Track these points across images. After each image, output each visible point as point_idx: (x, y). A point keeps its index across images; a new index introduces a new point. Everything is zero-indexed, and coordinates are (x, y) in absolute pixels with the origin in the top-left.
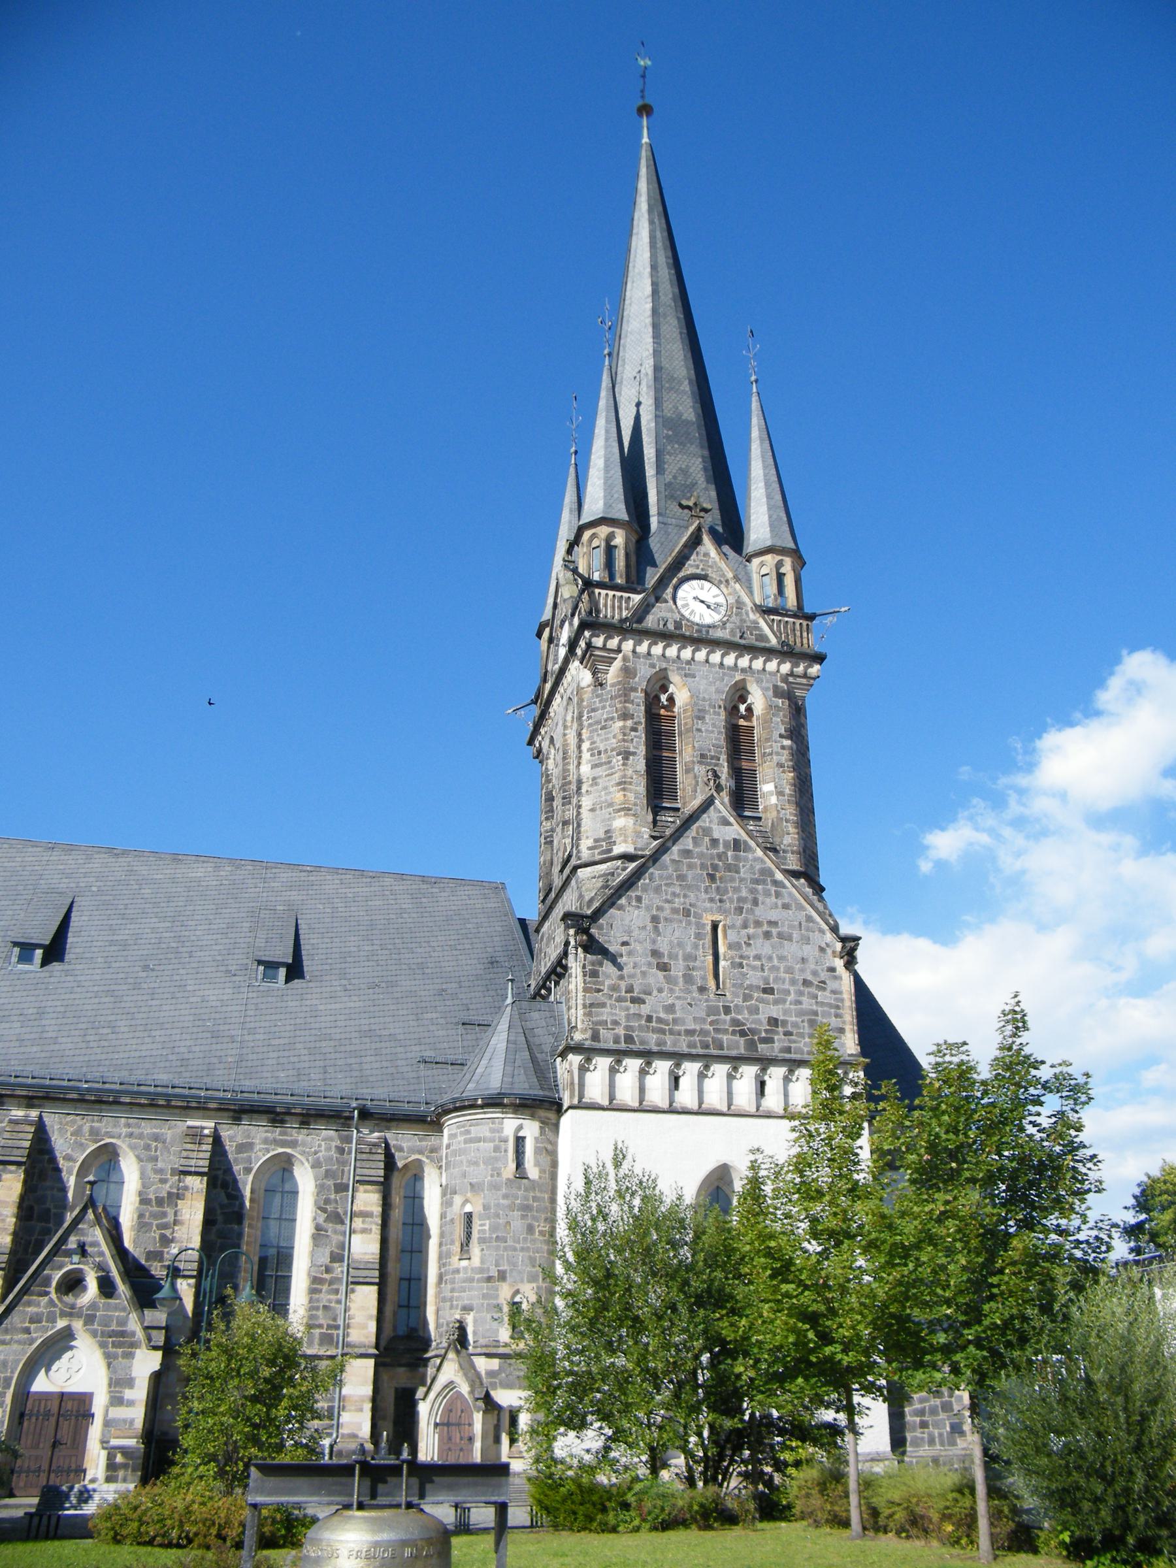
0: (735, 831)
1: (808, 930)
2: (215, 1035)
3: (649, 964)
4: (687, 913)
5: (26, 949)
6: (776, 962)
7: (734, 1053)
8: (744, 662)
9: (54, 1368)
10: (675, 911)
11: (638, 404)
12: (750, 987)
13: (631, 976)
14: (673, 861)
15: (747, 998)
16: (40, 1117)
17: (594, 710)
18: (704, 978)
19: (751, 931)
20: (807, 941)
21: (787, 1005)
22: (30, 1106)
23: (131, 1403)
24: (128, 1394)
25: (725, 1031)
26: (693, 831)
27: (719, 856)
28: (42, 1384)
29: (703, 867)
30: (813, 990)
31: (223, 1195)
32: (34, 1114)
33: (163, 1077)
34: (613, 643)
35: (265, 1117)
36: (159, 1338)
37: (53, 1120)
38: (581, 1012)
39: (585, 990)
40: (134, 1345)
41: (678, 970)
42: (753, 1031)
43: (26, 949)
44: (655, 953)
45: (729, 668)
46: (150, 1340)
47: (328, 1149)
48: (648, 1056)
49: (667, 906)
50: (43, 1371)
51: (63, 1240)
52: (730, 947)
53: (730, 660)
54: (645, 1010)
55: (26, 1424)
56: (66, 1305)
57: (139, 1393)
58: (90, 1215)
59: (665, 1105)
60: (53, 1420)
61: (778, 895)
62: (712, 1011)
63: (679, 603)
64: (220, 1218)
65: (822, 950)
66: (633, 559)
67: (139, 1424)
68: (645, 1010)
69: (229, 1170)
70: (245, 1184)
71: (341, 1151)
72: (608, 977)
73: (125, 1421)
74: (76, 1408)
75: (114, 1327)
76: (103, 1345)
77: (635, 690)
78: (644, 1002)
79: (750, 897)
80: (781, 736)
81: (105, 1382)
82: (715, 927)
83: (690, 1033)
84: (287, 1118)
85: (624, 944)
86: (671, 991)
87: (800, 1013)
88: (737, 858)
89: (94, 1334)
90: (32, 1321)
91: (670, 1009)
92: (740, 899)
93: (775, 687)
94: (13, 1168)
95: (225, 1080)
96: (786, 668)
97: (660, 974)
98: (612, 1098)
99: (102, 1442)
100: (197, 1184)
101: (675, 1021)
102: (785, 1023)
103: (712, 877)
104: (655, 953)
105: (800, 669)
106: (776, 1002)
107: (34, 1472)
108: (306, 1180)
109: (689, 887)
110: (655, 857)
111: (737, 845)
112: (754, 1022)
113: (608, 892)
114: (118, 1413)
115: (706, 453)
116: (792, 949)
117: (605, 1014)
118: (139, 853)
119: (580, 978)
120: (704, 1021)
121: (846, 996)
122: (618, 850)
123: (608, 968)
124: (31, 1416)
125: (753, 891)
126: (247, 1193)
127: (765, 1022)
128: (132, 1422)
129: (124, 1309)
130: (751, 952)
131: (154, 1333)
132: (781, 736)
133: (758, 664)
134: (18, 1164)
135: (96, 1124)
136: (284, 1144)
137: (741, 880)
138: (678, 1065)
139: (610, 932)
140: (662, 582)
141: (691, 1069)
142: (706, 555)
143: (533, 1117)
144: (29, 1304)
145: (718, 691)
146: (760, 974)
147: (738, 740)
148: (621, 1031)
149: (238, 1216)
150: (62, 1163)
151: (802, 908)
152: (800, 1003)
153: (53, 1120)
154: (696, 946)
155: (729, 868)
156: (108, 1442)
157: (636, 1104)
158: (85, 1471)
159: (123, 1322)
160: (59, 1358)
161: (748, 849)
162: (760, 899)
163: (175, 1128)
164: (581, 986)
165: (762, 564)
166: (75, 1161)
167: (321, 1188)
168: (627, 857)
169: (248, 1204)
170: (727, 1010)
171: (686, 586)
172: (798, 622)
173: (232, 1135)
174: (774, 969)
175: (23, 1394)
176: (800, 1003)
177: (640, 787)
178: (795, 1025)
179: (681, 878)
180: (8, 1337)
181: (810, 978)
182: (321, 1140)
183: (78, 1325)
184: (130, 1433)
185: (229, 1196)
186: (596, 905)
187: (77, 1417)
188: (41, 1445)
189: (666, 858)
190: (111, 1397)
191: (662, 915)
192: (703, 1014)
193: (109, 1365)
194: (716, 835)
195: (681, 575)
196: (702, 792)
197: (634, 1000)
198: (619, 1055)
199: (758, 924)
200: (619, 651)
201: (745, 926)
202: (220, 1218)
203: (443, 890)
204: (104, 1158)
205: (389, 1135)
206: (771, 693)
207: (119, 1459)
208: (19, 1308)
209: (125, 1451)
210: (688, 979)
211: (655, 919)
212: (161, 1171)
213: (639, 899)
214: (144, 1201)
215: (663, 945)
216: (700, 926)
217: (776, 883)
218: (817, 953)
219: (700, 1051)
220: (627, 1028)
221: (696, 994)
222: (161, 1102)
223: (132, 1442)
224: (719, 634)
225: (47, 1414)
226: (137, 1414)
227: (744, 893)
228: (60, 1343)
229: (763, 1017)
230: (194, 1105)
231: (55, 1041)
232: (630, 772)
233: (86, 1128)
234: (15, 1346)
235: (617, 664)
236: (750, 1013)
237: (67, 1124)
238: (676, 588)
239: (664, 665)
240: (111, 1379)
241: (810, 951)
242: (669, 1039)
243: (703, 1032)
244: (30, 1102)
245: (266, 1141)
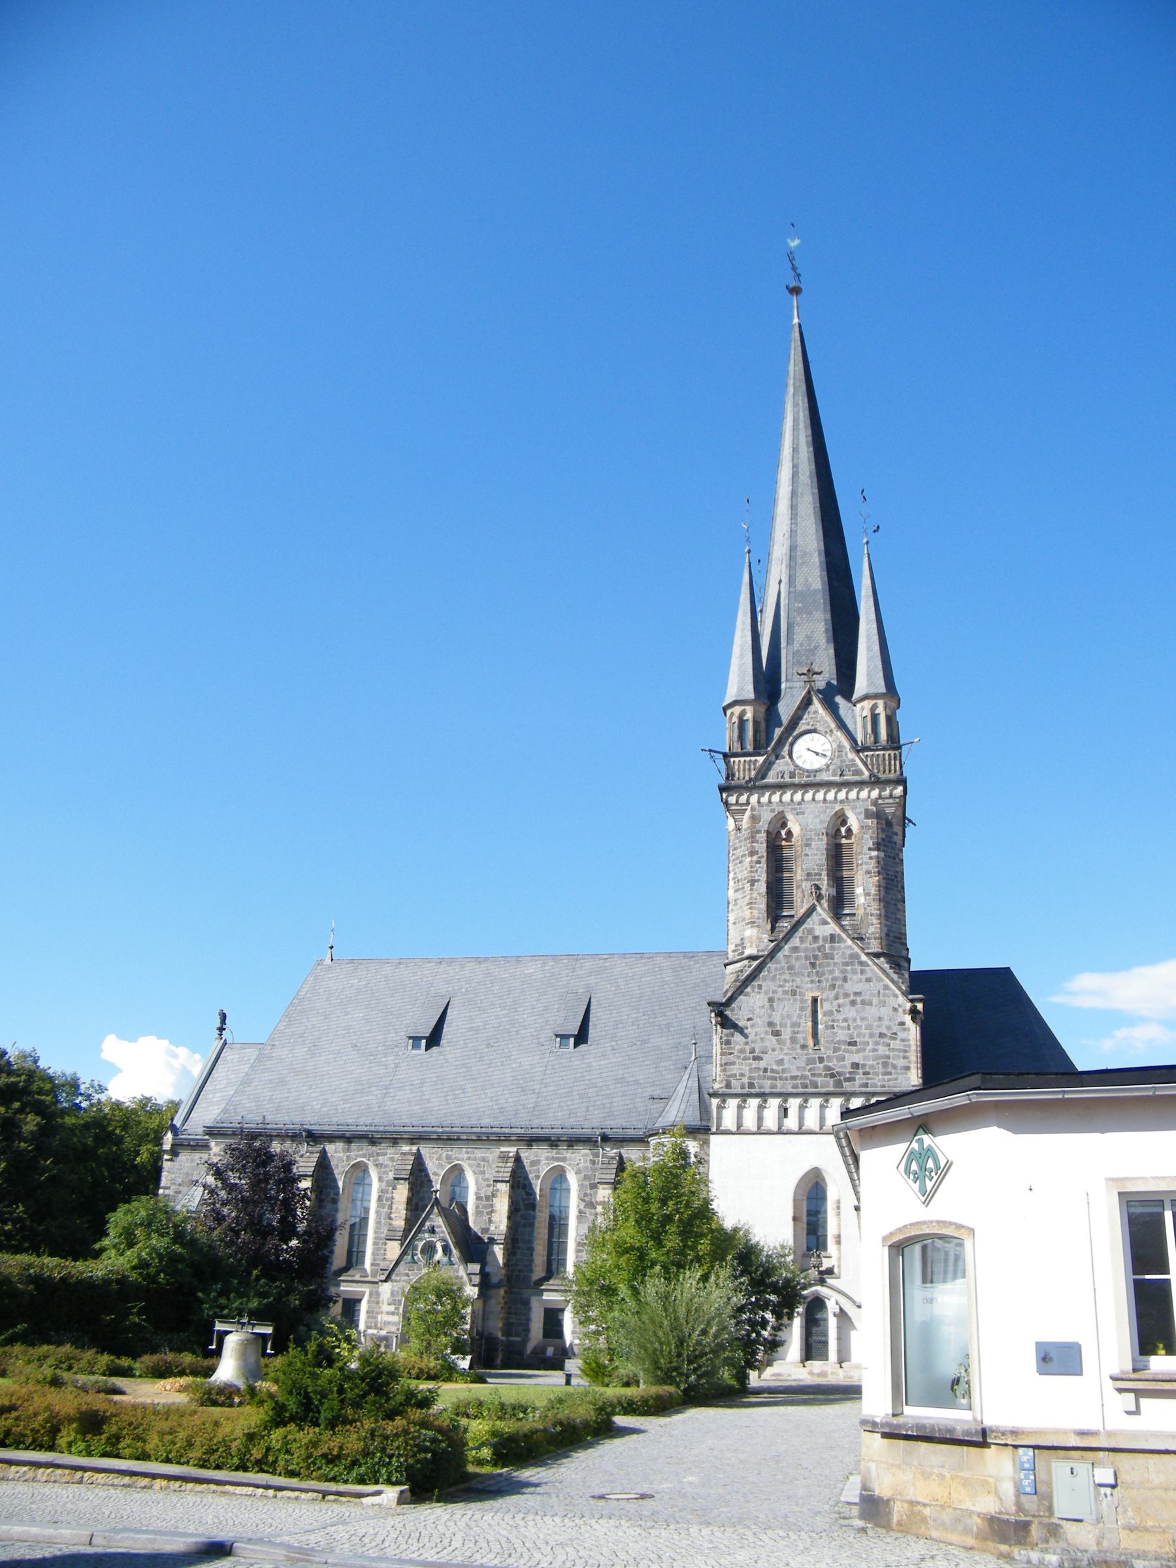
0: (832, 928)
1: (885, 995)
2: (524, 1090)
3: (766, 1033)
4: (794, 993)
5: (416, 1040)
6: (859, 1022)
7: (823, 1090)
8: (842, 795)
10: (785, 992)
11: (780, 582)
12: (839, 1042)
13: (753, 1042)
14: (785, 956)
15: (836, 1050)
16: (418, 1150)
17: (735, 849)
18: (805, 1039)
19: (841, 1001)
20: (884, 1004)
21: (866, 1053)
22: (412, 1144)
25: (820, 1075)
26: (799, 933)
27: (819, 949)
29: (807, 958)
30: (886, 1040)
31: (523, 1192)
32: (414, 1148)
33: (485, 1121)
34: (743, 799)
36: (477, 1280)
37: (427, 1151)
38: (719, 1069)
39: (722, 1054)
41: (786, 1034)
42: (840, 1074)
43: (416, 1040)
44: (770, 1024)
45: (831, 802)
47: (585, 1162)
48: (763, 1096)
49: (780, 989)
51: (422, 1224)
52: (825, 1014)
53: (831, 796)
54: (762, 1064)
58: (436, 1210)
59: (775, 1129)
61: (862, 972)
62: (810, 1061)
63: (795, 756)
64: (522, 1207)
65: (895, 1009)
66: (763, 725)
68: (762, 1064)
69: (526, 1178)
71: (593, 1162)
72: (737, 1043)
77: (759, 832)
78: (761, 1059)
79: (841, 976)
80: (870, 849)
82: (815, 1000)
83: (794, 1078)
85: (749, 1019)
86: (782, 1049)
87: (876, 1058)
88: (832, 948)
91: (780, 1062)
92: (834, 979)
93: (867, 811)
95: (526, 1120)
96: (875, 793)
97: (774, 1039)
98: (739, 1127)
100: (504, 1188)
101: (784, 1071)
102: (864, 1065)
103: (813, 965)
104: (770, 1024)
105: (887, 793)
106: (858, 1051)
108: (573, 1181)
109: (796, 974)
110: (772, 954)
111: (833, 938)
112: (841, 1067)
113: (738, 984)
115: (829, 616)
116: (872, 1012)
117: (735, 1070)
118: (494, 959)
119: (719, 1046)
120: (804, 1069)
121: (912, 1042)
122: (748, 952)
123: (738, 1037)
125: (842, 972)
126: (538, 1192)
127: (849, 1066)
130: (841, 1017)
132: (870, 849)
133: (853, 795)
136: (558, 1160)
137: (835, 964)
138: (785, 1101)
139: (739, 1013)
140: (781, 742)
141: (794, 1104)
142: (816, 712)
143: (695, 1139)
145: (822, 822)
146: (846, 1032)
147: (837, 857)
148: (746, 1080)
149: (532, 1206)
150: (432, 1177)
151: (881, 980)
152: (876, 1050)
153: (427, 1151)
154: (800, 1016)
155: (826, 956)
157: (755, 1129)
161: (841, 940)
162: (849, 976)
163: (493, 1153)
164: (719, 1051)
165: (863, 709)
167: (581, 1186)
168: (752, 958)
170: (821, 1060)
171: (796, 748)
172: (887, 753)
173: (527, 1155)
174: (857, 1027)
176: (876, 1050)
177: (762, 904)
178: (872, 1067)
179: (790, 968)
181: (885, 1031)
182: (580, 1157)
185: (527, 1194)
186: (729, 994)
189: (780, 955)
191: (776, 996)
192: (803, 1064)
194: (817, 933)
195: (795, 733)
196: (808, 902)
197: (755, 1058)
198: (744, 1097)
199: (846, 995)
200: (748, 803)
201: (837, 998)
202: (522, 1207)
203: (697, 962)
204: (456, 1172)
205: (622, 1151)
206: (863, 816)
210: (793, 1040)
211: (771, 1000)
212: (487, 1180)
213: (760, 987)
214: (478, 1198)
215: (777, 1019)
216: (803, 1001)
217: (861, 963)
218: (891, 1012)
219: (800, 1090)
220: (750, 1078)
221: (799, 1051)
224: (825, 777)
227: (837, 974)
229: (848, 1063)
231: (429, 1101)
232: (755, 895)
233: (444, 1155)
235: (748, 813)
236: (838, 1061)
238: (792, 745)
239: (781, 809)
241: (885, 1012)
242: (779, 1083)
243: (803, 1077)
244: (412, 1141)
245: (547, 1158)
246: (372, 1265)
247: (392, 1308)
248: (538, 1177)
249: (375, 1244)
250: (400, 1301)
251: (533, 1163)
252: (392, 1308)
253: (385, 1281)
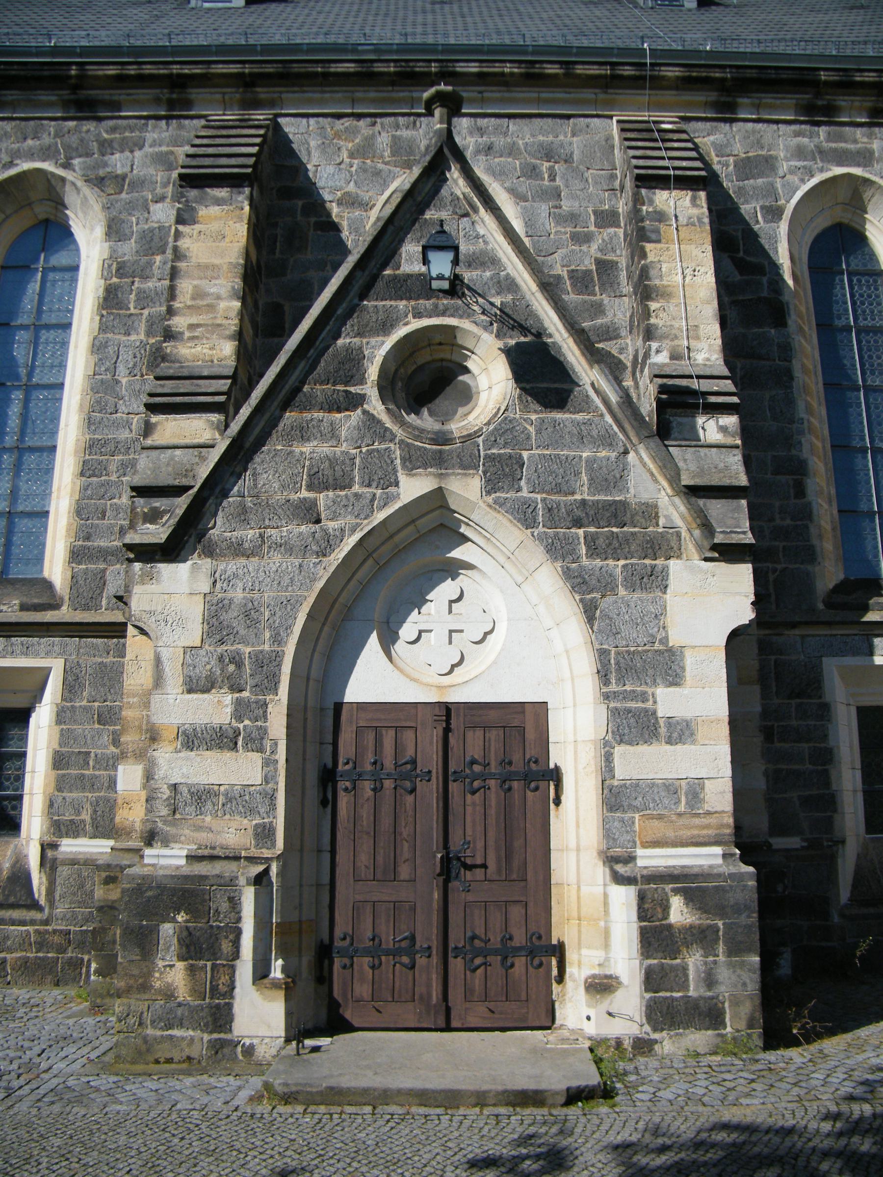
9: (407, 631)
23: (681, 732)
24: (668, 702)
28: (373, 679)
35: (790, 100)
40: (662, 546)
46: (707, 527)
50: (373, 640)
55: (344, 801)
56: (419, 433)
57: (703, 695)
60: (430, 790)
67: (720, 796)
70: (774, 240)
73: (671, 788)
74: (496, 758)
75: (583, 494)
76: (558, 550)
81: (584, 664)
84: (842, 101)
89: (525, 516)
90: (317, 483)
94: (222, 193)
99: (611, 860)
107: (395, 953)
114: (638, 763)
124: (356, 778)
126: (783, 257)
128: (695, 790)
129: (607, 440)
131: (715, 508)
134: (233, 181)
135: (405, 133)
136: (842, 158)
144: (303, 433)
156: (630, 859)
158: (559, 951)
159: (615, 478)
160: (419, 601)
166: (367, 206)
169: (790, 282)
175: (321, 716)
180: (251, 534)
183: (466, 490)
184: (693, 827)
187: (505, 780)
188: (404, 871)
190: (615, 713)
193: (590, 612)
207: (679, 912)
208: (275, 445)
209: (689, 884)
212: (573, 218)
222: (552, 70)
223: (708, 858)
225: (408, 773)
226: (707, 763)
228: (407, 561)
230: (628, 71)
233: (383, 140)
234: (276, 560)
237: (337, 135)
240: (602, 654)
245: (800, 153)
246: (76, 555)
247: (216, 709)
248: (774, 213)
249: (87, 470)
250: (267, 666)
251: (748, 167)
252: (216, 709)
253: (171, 550)
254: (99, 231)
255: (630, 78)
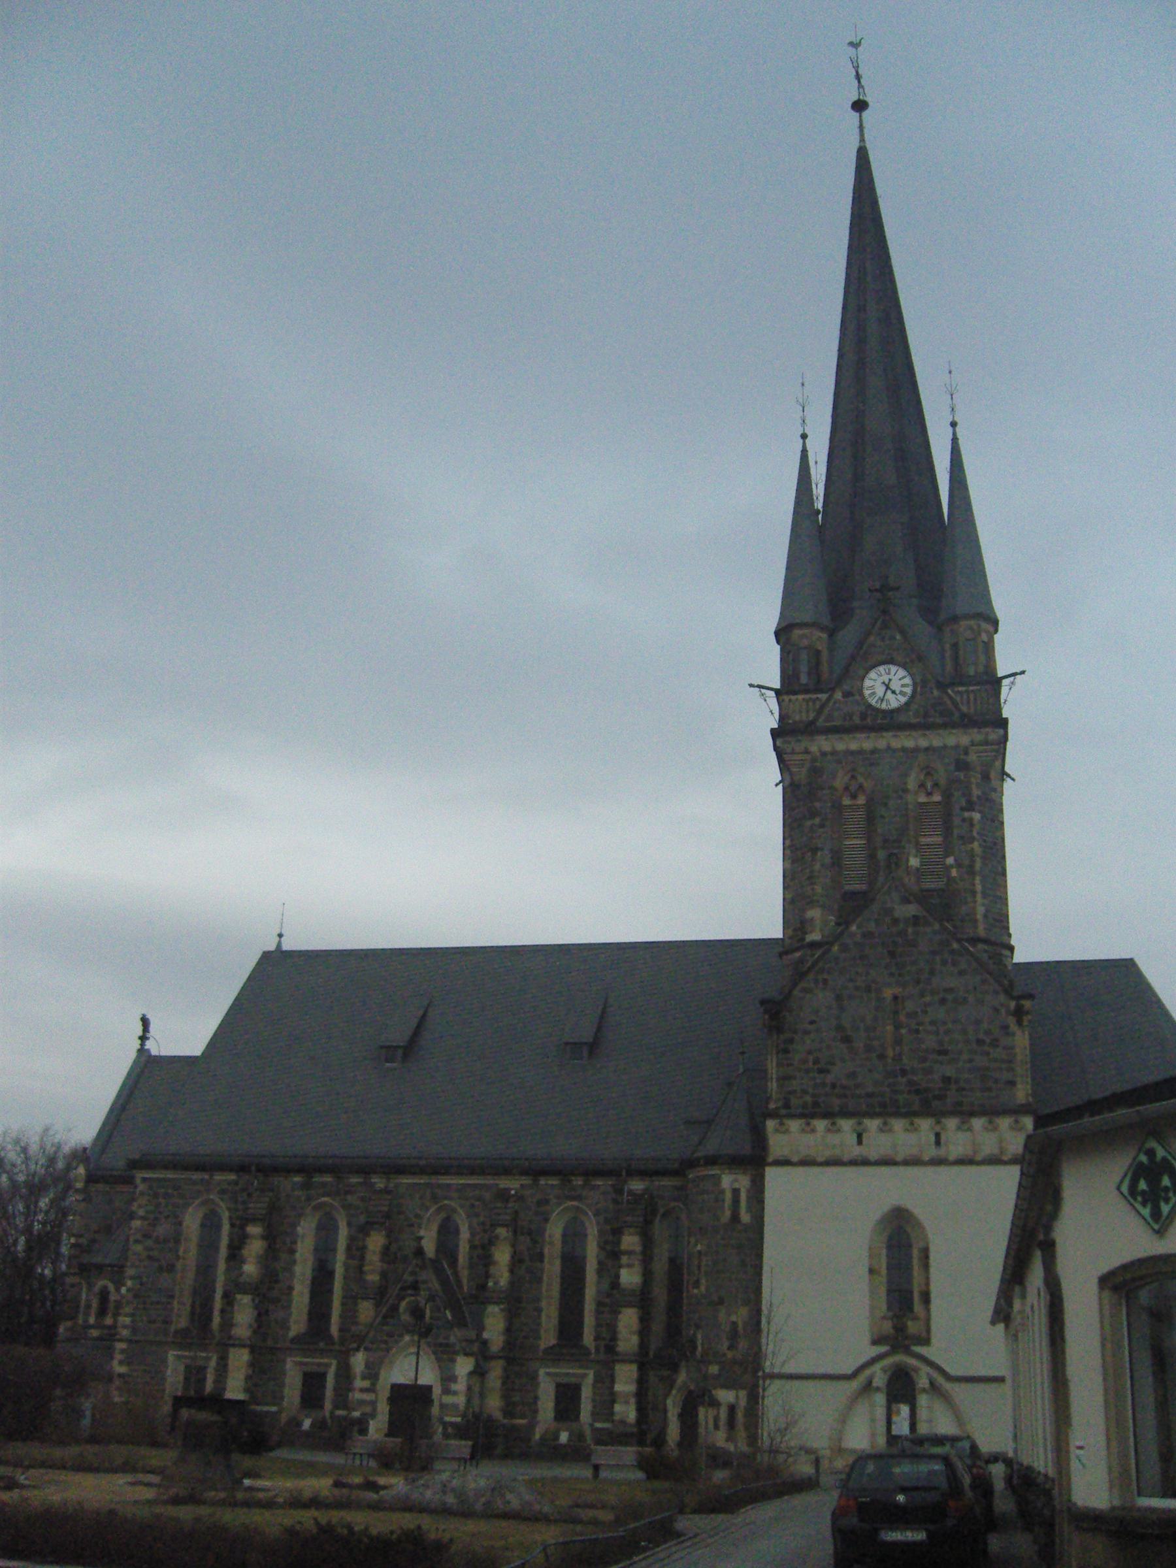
23: (455, 1393)
24: (454, 1387)
40: (456, 1353)
76: (434, 1353)
207: (450, 1430)
209: (452, 1424)
254: (345, 1224)
255: (507, 1172)
